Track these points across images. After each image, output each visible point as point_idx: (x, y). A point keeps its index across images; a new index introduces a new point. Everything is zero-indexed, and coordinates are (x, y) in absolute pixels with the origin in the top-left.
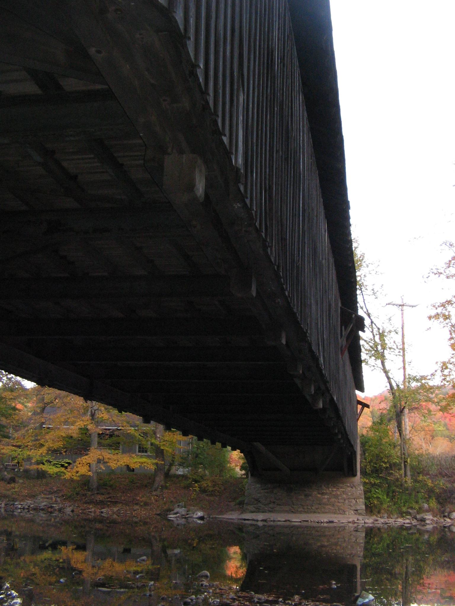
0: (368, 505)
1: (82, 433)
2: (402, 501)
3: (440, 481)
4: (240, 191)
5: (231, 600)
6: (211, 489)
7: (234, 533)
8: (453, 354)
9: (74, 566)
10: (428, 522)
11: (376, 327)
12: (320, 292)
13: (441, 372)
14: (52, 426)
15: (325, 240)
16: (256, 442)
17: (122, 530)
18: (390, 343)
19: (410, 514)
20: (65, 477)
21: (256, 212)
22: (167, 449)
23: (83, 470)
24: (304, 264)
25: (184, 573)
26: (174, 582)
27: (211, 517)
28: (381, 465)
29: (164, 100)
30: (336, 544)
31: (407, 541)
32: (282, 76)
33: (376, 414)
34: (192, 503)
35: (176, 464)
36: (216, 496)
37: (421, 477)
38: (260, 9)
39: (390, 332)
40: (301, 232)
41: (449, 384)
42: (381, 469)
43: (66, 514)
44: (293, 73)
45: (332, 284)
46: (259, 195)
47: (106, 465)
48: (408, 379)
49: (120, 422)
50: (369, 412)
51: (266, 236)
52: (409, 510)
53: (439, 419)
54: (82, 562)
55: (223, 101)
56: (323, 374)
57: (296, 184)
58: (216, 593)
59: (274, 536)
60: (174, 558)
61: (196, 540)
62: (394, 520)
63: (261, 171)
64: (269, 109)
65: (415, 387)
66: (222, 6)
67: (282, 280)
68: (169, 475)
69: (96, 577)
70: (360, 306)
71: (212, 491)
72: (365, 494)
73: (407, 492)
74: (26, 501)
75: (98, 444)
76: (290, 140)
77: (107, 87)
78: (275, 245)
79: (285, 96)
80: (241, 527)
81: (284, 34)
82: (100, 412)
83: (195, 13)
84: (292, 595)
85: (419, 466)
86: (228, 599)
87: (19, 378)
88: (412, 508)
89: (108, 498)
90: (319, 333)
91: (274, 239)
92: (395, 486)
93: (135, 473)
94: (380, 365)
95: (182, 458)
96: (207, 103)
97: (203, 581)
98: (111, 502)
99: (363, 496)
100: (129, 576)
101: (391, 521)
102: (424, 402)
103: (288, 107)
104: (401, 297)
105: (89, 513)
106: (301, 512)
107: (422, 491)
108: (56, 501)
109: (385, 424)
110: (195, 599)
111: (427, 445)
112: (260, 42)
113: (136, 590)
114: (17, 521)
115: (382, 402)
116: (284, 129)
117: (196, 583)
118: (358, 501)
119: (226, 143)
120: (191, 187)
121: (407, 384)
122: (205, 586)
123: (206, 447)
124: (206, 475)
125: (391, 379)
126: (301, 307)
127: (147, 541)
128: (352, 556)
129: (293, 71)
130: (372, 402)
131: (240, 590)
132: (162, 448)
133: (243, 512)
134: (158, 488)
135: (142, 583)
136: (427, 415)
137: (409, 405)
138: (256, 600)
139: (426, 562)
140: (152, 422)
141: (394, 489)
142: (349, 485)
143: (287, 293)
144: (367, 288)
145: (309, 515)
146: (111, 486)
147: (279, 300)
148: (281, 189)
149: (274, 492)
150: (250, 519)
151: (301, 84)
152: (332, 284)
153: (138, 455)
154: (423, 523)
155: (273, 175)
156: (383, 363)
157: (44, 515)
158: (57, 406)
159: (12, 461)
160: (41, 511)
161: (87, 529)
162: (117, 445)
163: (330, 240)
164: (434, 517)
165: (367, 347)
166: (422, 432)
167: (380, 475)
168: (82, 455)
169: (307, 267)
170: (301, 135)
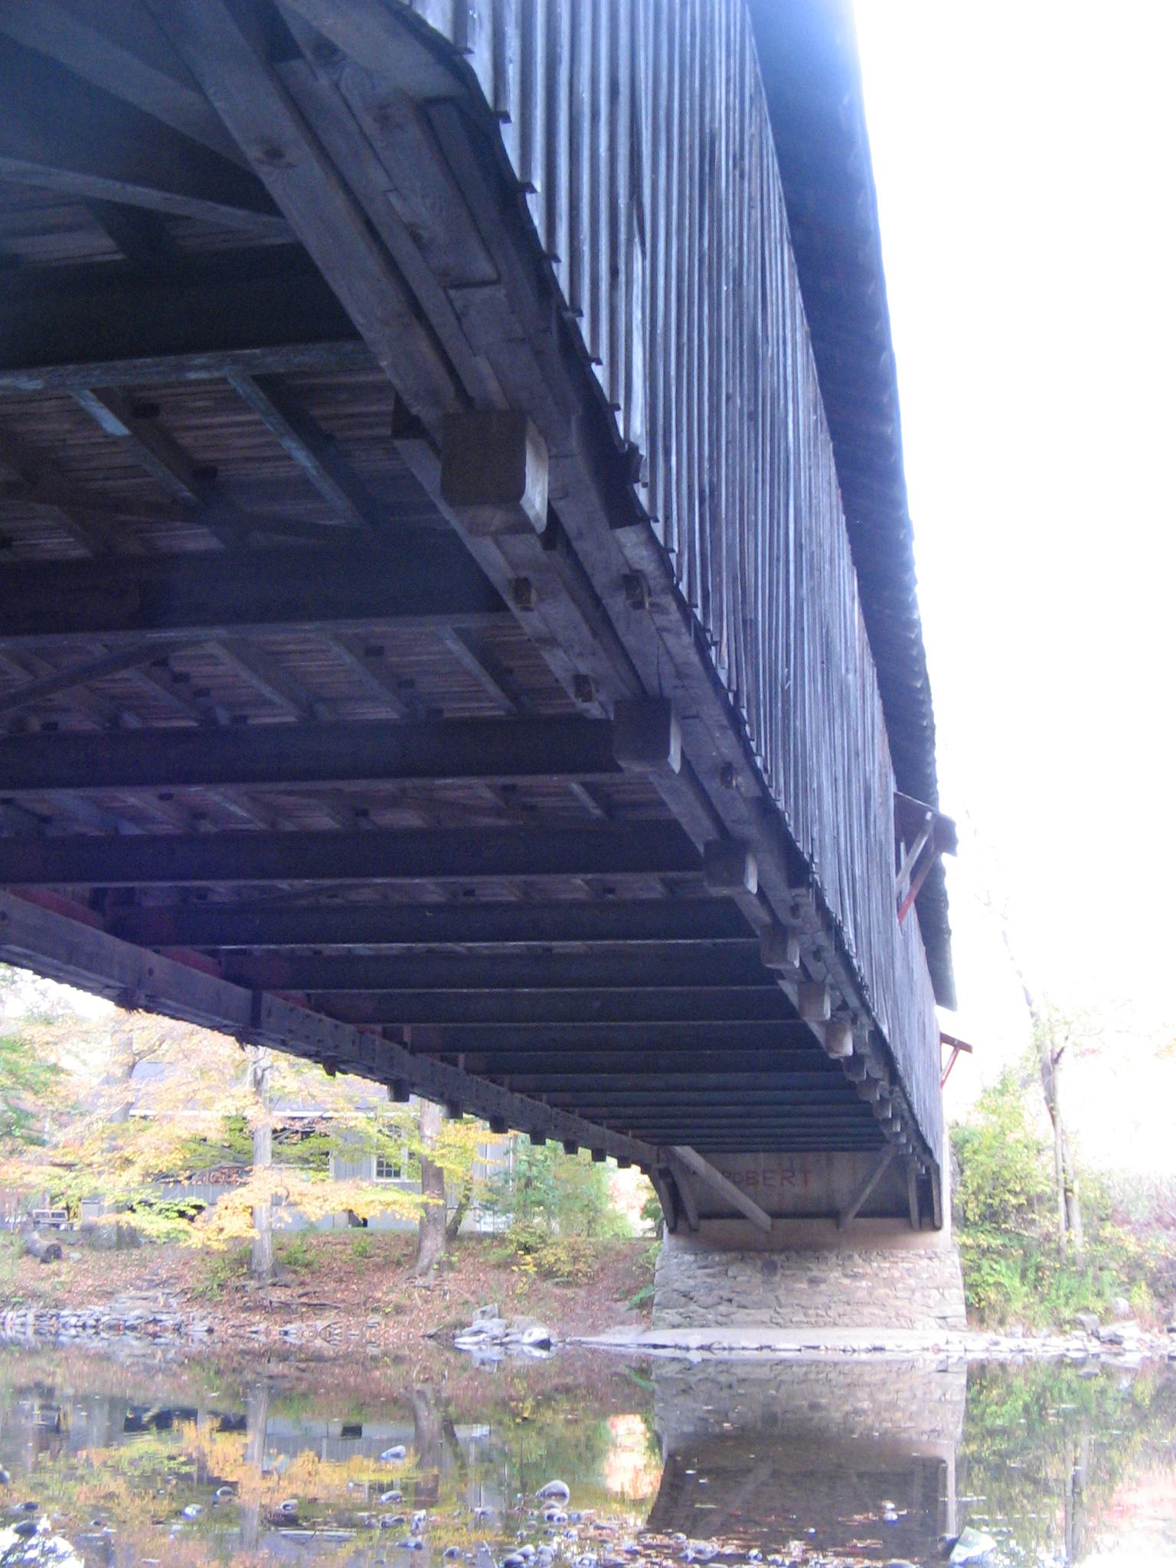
1: (231, 1130)
2: (1061, 1293)
3: (1157, 1240)
5: (629, 1557)
6: (567, 1268)
7: (629, 1383)
10: (1126, 1345)
22: (452, 1167)
23: (236, 1225)
26: (479, 1510)
27: (568, 1340)
30: (892, 1406)
35: (476, 1204)
36: (579, 1286)
37: (1108, 1230)
42: (1004, 1209)
47: (294, 1210)
61: (530, 1403)
71: (570, 1273)
72: (965, 1275)
73: (1073, 1269)
74: (90, 1307)
80: (644, 1365)
82: (277, 1074)
84: (784, 1540)
85: (1104, 1201)
86: (618, 1553)
88: (1087, 1310)
89: (301, 1296)
92: (1042, 1254)
97: (552, 1507)
98: (310, 1305)
99: (960, 1282)
105: (254, 1336)
106: (799, 1325)
107: (1113, 1265)
108: (167, 1305)
118: (946, 1293)
122: (559, 1519)
124: (552, 1233)
127: (401, 1406)
132: (438, 1164)
133: (652, 1325)
134: (429, 1267)
138: (691, 1554)
140: (412, 1097)
149: (730, 1273)
153: (377, 1185)
154: (1115, 1348)
157: (135, 1343)
158: (167, 1059)
161: (249, 1376)
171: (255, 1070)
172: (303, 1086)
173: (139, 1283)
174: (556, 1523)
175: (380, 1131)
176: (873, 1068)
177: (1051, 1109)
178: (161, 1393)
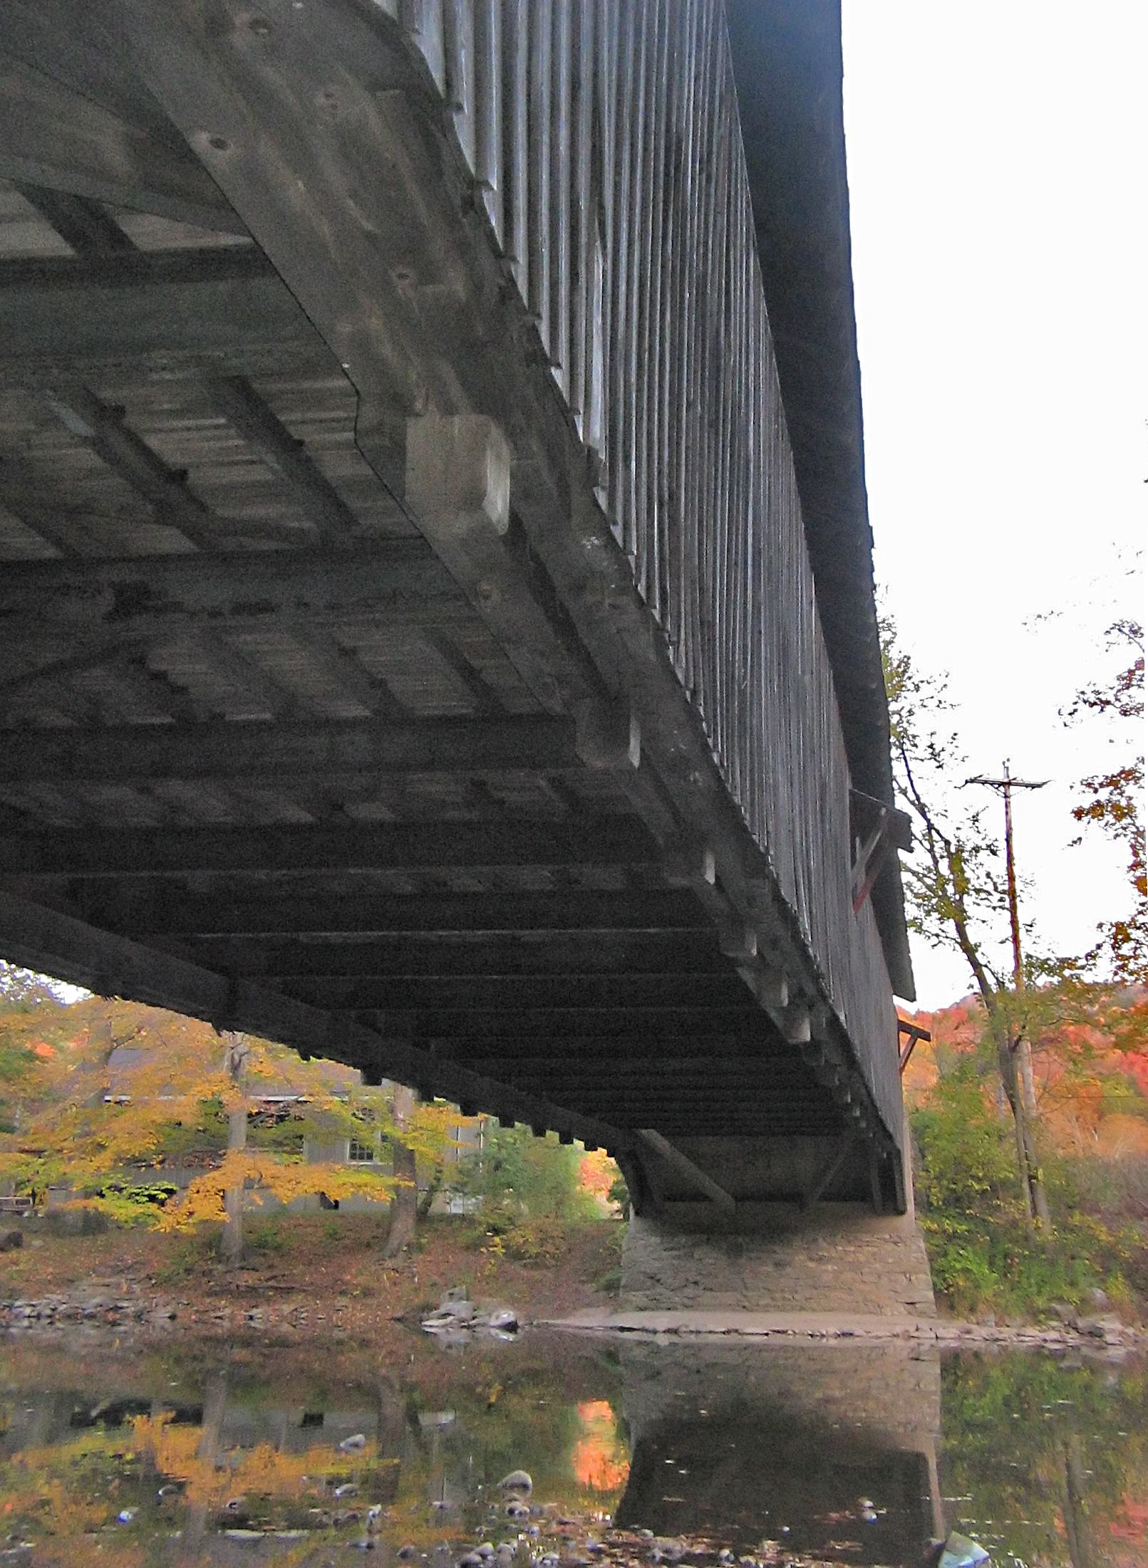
0: (941, 1291)
2: (1033, 1281)
3: (1131, 1229)
4: (598, 506)
5: (592, 1555)
6: (534, 1250)
7: (596, 1366)
8: (1143, 904)
9: (165, 1472)
10: (1109, 1338)
11: (939, 839)
12: (798, 753)
13: (1114, 949)
14: (128, 1098)
15: (810, 626)
16: (646, 1128)
17: (302, 1362)
18: (978, 878)
19: (1057, 1315)
20: (159, 1227)
21: (638, 558)
22: (422, 1148)
23: (207, 1209)
24: (759, 686)
25: (465, 1479)
26: (437, 1503)
27: (535, 1323)
28: (968, 1186)
29: (401, 276)
30: (865, 1395)
31: (1058, 1389)
32: (703, 209)
33: (949, 1054)
34: (487, 1287)
37: (1076, 1219)
38: (648, 20)
39: (977, 849)
40: (750, 607)
41: (1137, 979)
42: (968, 1196)
43: (154, 1327)
44: (732, 200)
45: (829, 733)
46: (644, 515)
47: (266, 1192)
48: (1026, 966)
49: (304, 1083)
50: (928, 1052)
51: (663, 616)
52: (1053, 1305)
53: (1115, 1069)
54: (188, 1457)
55: (551, 276)
56: (809, 957)
57: (738, 485)
58: (550, 1536)
59: (698, 1372)
60: (437, 1437)
61: (497, 1387)
62: (1015, 1331)
63: (649, 456)
64: (668, 296)
65: (1045, 987)
66: (544, 12)
67: (704, 725)
68: (428, 1214)
69: (224, 1499)
70: (900, 788)
71: (538, 1254)
72: (931, 1260)
73: (1044, 1256)
74: (47, 1296)
75: (247, 1139)
76: (722, 375)
77: (248, 240)
78: (686, 640)
79: (710, 262)
80: (612, 1348)
81: (713, 92)
82: (254, 1059)
83: (471, 34)
84: (757, 1541)
86: (581, 1552)
87: (44, 978)
88: (1060, 1299)
90: (798, 856)
91: (683, 624)
92: (1010, 1241)
93: (340, 1211)
94: (953, 933)
95: (461, 1172)
96: (512, 281)
97: (516, 1500)
98: (276, 1288)
99: (927, 1267)
100: (314, 1491)
101: (1007, 1333)
102: (1071, 1024)
103: (720, 289)
104: (1004, 763)
105: (218, 1321)
106: (766, 1308)
107: (1085, 1254)
108: (130, 1292)
109: (971, 1082)
110: (493, 1554)
111: (1088, 1134)
112: (647, 117)
113: (332, 1532)
114: (15, 1352)
115: (961, 1026)
116: (708, 346)
117: (497, 1506)
118: (913, 1278)
119: (560, 386)
120: (474, 499)
121: (1025, 979)
122: (520, 1514)
123: (521, 1142)
124: (521, 1215)
125: (984, 969)
126: (752, 793)
127: (368, 1394)
128: (910, 1427)
129: (733, 193)
130: (936, 1026)
131: (616, 1526)
133: (618, 1308)
134: (398, 1250)
135: (350, 1509)
136: (1081, 1058)
137: (1031, 1033)
138: (659, 1554)
139: (1122, 1454)
140: (385, 1081)
141: (1008, 1249)
142: (887, 1237)
143: (716, 759)
144: (917, 741)
145: (790, 1317)
146: (277, 1248)
147: (697, 774)
148: (701, 500)
149: (696, 1256)
150: (635, 1327)
151: (752, 227)
152: (829, 733)
153: (350, 1166)
154: (1096, 1341)
155: (678, 464)
156: (961, 929)
157: (93, 1332)
158: (145, 1045)
159: (16, 1190)
160: (85, 1321)
161: (209, 1364)
162: (297, 1140)
163: (823, 624)
164: (1126, 1327)
165: (918, 887)
166: (1071, 1101)
167: (968, 1212)
168: (203, 1168)
169: (766, 692)
170: (752, 361)
171: (232, 1056)
172: (279, 1071)
173: (102, 1269)
174: (517, 1518)
175: (354, 1114)
176: (830, 1054)
177: (1010, 1097)
178: (118, 1384)
